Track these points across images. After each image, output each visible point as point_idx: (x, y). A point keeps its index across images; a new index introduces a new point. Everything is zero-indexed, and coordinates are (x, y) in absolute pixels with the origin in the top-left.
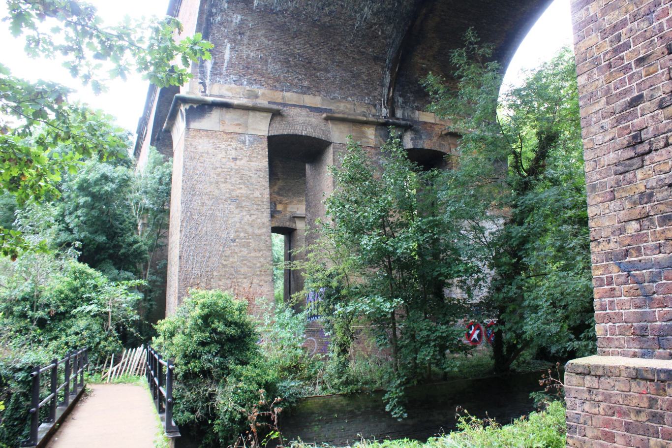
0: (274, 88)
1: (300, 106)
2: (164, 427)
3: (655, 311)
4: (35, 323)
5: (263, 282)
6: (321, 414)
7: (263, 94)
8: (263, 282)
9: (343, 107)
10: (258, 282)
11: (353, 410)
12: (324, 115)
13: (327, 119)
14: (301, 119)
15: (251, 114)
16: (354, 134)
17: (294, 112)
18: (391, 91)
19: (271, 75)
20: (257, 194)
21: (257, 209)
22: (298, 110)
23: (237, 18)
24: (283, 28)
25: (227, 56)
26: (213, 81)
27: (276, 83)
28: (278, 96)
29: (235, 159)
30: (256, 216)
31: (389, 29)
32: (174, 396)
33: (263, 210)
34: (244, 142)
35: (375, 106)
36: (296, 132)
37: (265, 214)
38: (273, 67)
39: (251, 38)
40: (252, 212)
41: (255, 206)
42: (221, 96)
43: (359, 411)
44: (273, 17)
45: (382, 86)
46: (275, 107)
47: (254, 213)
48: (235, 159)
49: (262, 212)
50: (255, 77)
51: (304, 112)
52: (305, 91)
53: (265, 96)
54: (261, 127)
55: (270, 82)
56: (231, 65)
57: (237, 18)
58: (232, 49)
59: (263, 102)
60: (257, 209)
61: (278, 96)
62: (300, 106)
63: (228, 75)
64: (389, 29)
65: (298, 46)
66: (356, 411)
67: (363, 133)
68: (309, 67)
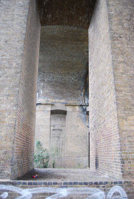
0: (53, 99)
1: (59, 103)
7: (50, 100)
9: (71, 102)
12: (65, 104)
13: (66, 105)
14: (59, 106)
15: (46, 105)
16: (73, 108)
17: (57, 104)
20: (47, 124)
22: (59, 103)
23: (42, 84)
24: (53, 85)
25: (41, 92)
26: (38, 99)
27: (54, 98)
28: (54, 101)
29: (42, 116)
31: (80, 82)
32: (128, 190)
34: (45, 112)
35: (79, 101)
36: (58, 109)
38: (52, 94)
39: (46, 88)
42: (40, 102)
44: (50, 83)
45: (81, 96)
46: (52, 104)
48: (42, 116)
50: (48, 96)
51: (60, 104)
52: (61, 99)
53: (51, 101)
54: (49, 108)
55: (52, 97)
56: (43, 94)
57: (42, 84)
58: (42, 91)
59: (50, 102)
61: (54, 101)
62: (59, 103)
63: (42, 97)
64: (80, 82)
65: (58, 88)
67: (75, 108)
68: (62, 93)
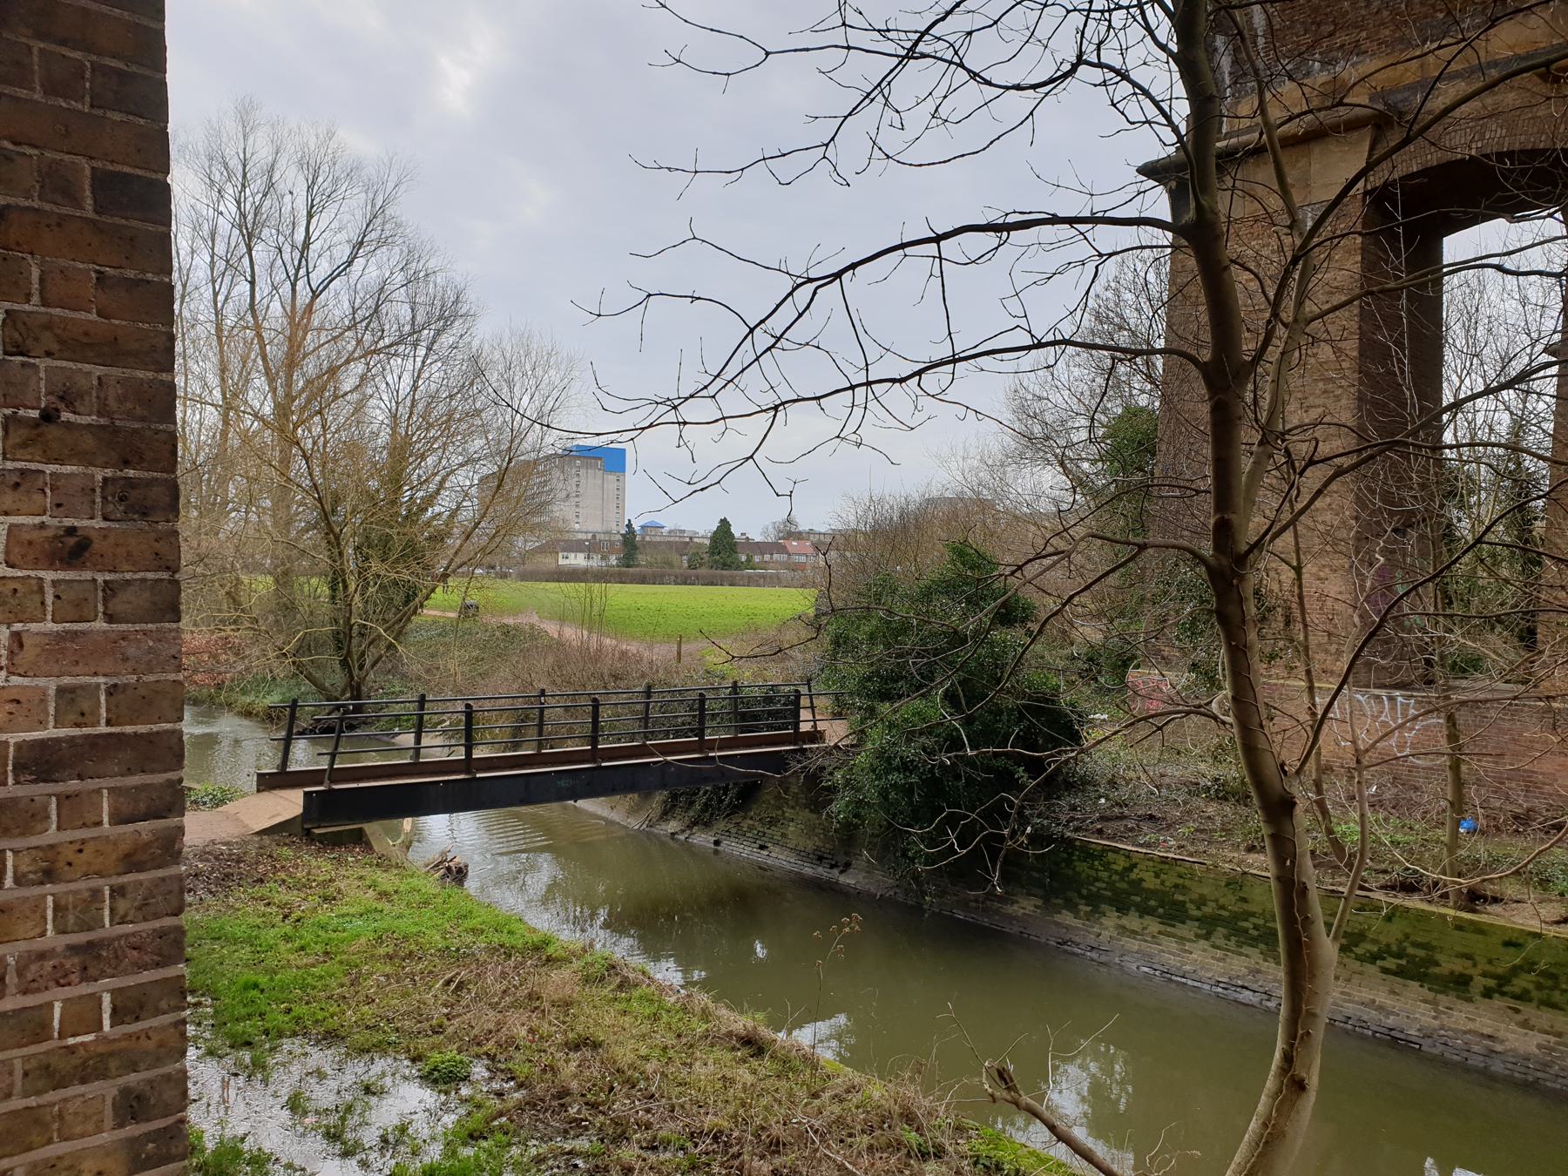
2: (339, 861)
3: (109, 723)
4: (603, 914)
5: (1327, 570)
6: (683, 831)
8: (1327, 570)
10: (1315, 570)
11: (1185, 902)
15: (1316, 149)
18: (1265, 404)
19: (1385, 13)
21: (1325, 392)
30: (1320, 410)
33: (1339, 391)
37: (1344, 402)
40: (1311, 400)
41: (1321, 384)
43: (1199, 908)
47: (1318, 402)
49: (1338, 398)
60: (1325, 392)
66: (1193, 907)
